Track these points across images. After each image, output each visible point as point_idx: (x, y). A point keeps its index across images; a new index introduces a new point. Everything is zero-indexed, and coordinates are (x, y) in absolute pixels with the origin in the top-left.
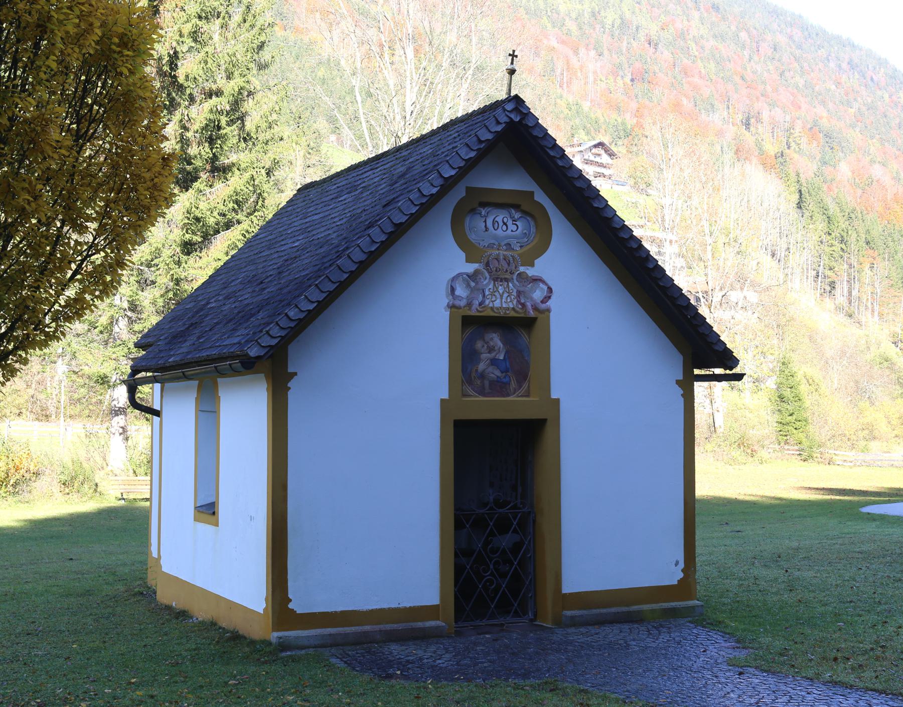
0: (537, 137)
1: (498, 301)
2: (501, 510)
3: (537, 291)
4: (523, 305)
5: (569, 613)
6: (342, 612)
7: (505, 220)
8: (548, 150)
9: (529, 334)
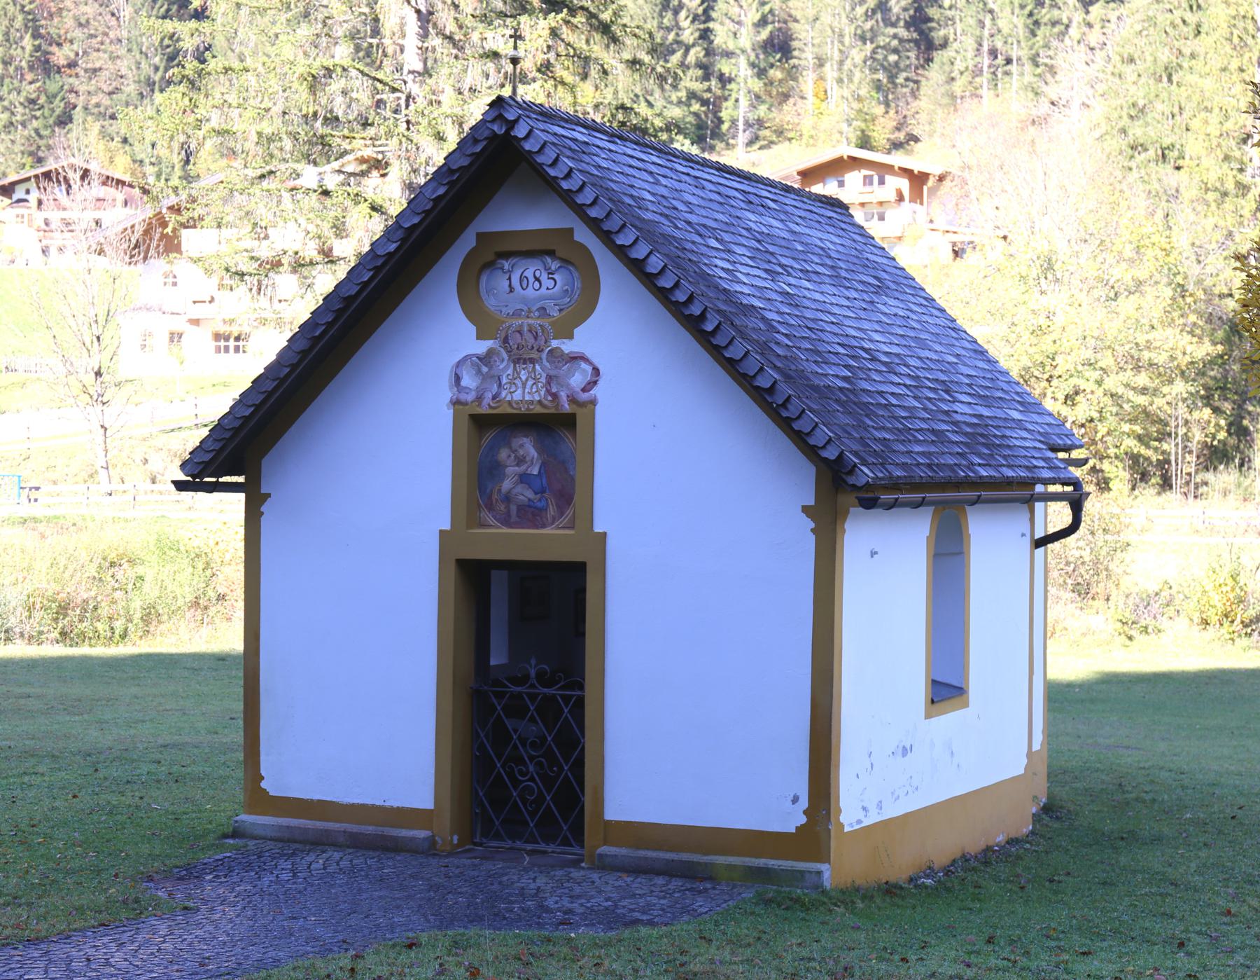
0: (530, 152)
1: (519, 391)
2: (545, 690)
3: (576, 374)
7: (538, 274)
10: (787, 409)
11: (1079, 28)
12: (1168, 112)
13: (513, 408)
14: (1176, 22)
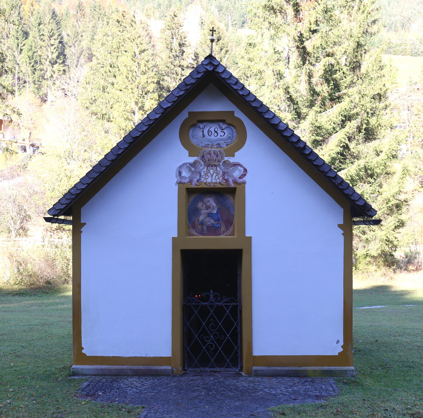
0: (224, 78)
1: (210, 178)
2: (203, 303)
4: (227, 180)
5: (254, 368)
6: (112, 357)
7: (216, 130)
8: (232, 86)
9: (234, 198)
10: (342, 185)
11: (50, 72)
12: (104, 102)
13: (207, 185)
14: (107, 71)
